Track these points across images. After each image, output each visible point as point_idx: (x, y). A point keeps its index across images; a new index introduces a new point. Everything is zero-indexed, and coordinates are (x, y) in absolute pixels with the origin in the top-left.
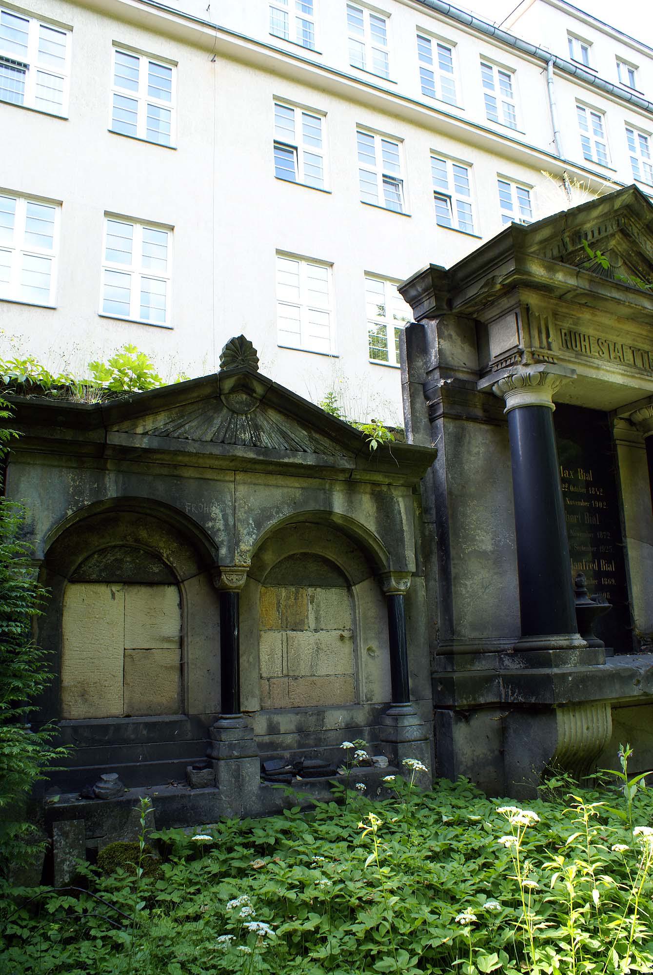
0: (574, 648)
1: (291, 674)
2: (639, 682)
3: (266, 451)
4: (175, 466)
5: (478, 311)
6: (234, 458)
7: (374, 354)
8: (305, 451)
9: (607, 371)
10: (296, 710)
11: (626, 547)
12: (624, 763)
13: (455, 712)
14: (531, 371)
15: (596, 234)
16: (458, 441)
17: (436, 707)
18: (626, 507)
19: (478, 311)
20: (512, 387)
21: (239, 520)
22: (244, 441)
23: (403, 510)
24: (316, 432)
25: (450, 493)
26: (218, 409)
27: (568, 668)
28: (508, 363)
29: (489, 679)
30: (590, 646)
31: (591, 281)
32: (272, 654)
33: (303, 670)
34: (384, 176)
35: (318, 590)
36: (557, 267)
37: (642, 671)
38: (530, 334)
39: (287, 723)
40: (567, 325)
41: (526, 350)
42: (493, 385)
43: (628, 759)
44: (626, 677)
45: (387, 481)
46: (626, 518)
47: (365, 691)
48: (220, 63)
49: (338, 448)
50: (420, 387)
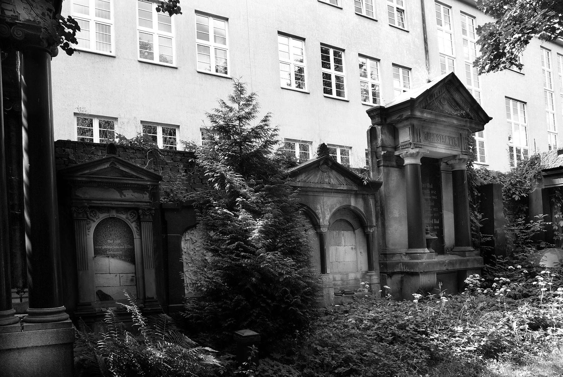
3: (333, 185)
4: (307, 192)
7: (326, 91)
9: (439, 148)
10: (340, 273)
12: (440, 287)
16: (387, 175)
17: (380, 273)
20: (407, 156)
22: (326, 182)
24: (347, 177)
25: (385, 196)
30: (431, 252)
39: (338, 277)
40: (426, 130)
50: (374, 153)
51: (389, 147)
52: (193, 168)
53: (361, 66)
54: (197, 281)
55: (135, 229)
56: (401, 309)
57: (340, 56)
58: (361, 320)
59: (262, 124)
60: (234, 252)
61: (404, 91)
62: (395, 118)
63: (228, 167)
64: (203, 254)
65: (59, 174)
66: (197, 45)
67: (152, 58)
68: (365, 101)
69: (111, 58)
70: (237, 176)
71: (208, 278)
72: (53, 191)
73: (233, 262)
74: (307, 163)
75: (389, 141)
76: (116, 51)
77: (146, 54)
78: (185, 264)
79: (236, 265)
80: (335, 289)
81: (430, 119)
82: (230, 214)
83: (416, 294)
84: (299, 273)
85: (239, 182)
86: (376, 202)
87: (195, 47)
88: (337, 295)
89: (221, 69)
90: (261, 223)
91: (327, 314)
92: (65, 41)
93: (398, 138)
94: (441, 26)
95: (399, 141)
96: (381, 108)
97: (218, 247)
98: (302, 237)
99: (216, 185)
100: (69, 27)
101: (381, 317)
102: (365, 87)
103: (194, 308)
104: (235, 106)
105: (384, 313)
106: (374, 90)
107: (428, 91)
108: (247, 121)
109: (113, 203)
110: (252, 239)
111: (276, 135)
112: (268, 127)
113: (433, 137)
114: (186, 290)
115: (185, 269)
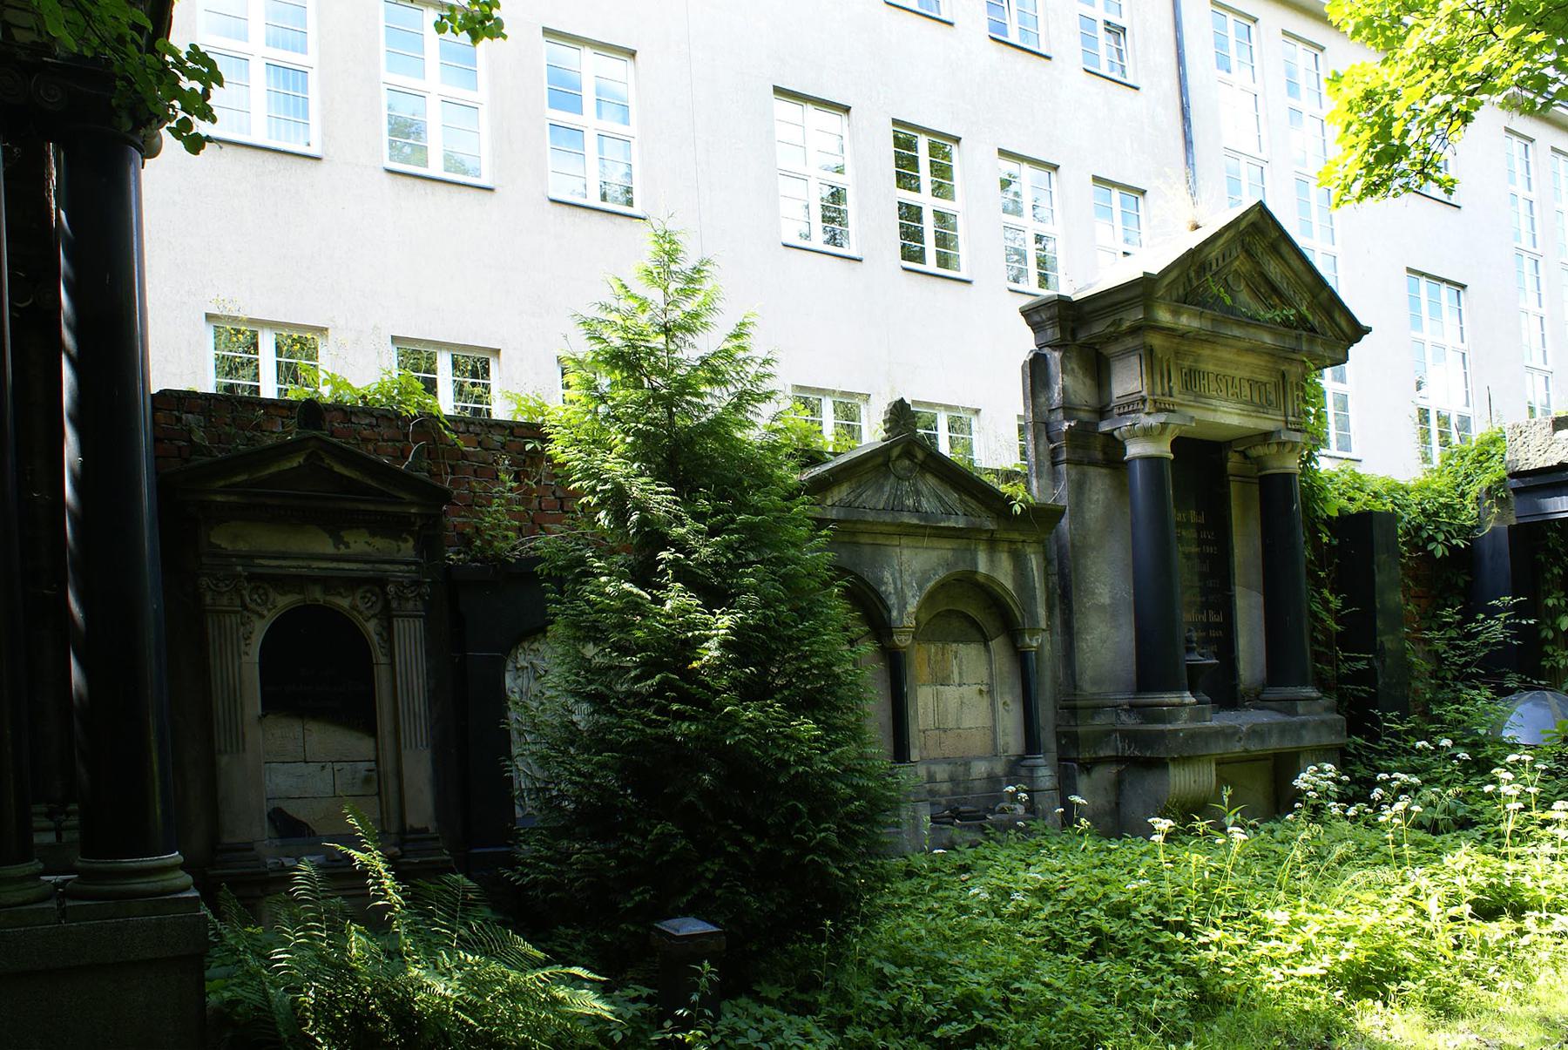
0: (1183, 705)
2: (1241, 739)
3: (925, 516)
4: (854, 533)
5: (1101, 343)
6: (900, 525)
7: (907, 254)
8: (957, 514)
10: (947, 760)
11: (1234, 596)
12: (1226, 800)
14: (1153, 421)
16: (1079, 488)
17: (1059, 760)
18: (1236, 551)
19: (1101, 343)
21: (907, 584)
22: (909, 507)
25: (1073, 545)
26: (886, 477)
27: (1179, 725)
29: (1108, 734)
30: (1199, 703)
36: (1182, 310)
37: (1244, 729)
39: (941, 772)
41: (1149, 398)
43: (1229, 797)
44: (1228, 734)
45: (1022, 538)
46: (1236, 564)
49: (983, 509)
52: (537, 467)
53: (1005, 184)
54: (548, 783)
55: (376, 638)
56: (1118, 860)
57: (947, 156)
59: (727, 345)
60: (653, 703)
62: (1099, 328)
63: (635, 466)
64: (564, 706)
65: (165, 487)
70: (660, 489)
71: (579, 773)
73: (648, 731)
75: (1082, 391)
77: (407, 150)
78: (514, 736)
79: (658, 738)
80: (932, 804)
82: (639, 596)
83: (1158, 819)
84: (834, 762)
85: (666, 507)
86: (1048, 561)
88: (938, 823)
91: (909, 874)
92: (181, 115)
96: (1063, 303)
97: (606, 687)
98: (841, 659)
99: (602, 514)
100: (192, 75)
103: (541, 858)
104: (656, 296)
106: (1041, 250)
107: (1191, 253)
108: (689, 337)
109: (315, 564)
110: (703, 667)
111: (770, 375)
112: (748, 354)
114: (517, 809)
115: (515, 751)
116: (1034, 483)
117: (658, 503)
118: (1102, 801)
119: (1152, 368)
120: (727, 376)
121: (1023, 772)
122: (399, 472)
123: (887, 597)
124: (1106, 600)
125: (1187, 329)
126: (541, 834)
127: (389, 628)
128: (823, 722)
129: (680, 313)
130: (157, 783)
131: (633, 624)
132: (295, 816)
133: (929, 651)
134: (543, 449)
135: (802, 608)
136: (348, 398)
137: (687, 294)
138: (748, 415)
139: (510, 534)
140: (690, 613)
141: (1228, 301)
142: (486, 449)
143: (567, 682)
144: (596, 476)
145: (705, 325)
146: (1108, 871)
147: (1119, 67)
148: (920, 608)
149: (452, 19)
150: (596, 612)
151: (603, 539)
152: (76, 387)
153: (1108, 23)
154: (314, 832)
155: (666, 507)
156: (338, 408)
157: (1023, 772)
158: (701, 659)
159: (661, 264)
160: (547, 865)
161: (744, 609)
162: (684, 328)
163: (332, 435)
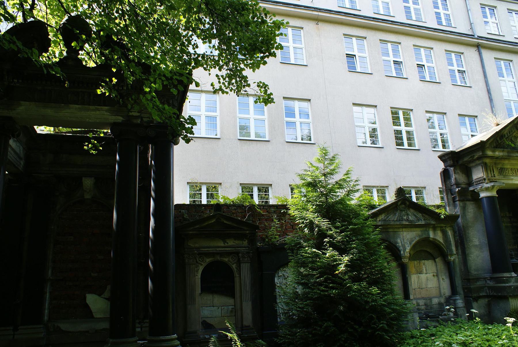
0: (513, 277)
1: (420, 287)
3: (411, 221)
8: (421, 220)
10: (423, 298)
13: (472, 298)
14: (489, 185)
15: (508, 134)
16: (464, 208)
17: (465, 297)
20: (482, 190)
21: (405, 243)
22: (405, 219)
23: (450, 234)
25: (463, 226)
26: (397, 210)
28: (480, 182)
31: (508, 152)
32: (414, 281)
33: (424, 286)
34: (394, 61)
35: (426, 261)
38: (487, 173)
39: (422, 302)
40: (499, 166)
42: (475, 189)
45: (445, 226)
47: (443, 292)
48: (320, 24)
50: (449, 191)
51: (463, 184)
52: (285, 217)
53: (428, 120)
54: (289, 311)
55: (235, 269)
56: (493, 332)
57: (409, 115)
58: (450, 344)
59: (344, 177)
60: (324, 285)
61: (472, 136)
62: (466, 159)
63: (316, 214)
64: (294, 287)
65: (176, 230)
66: (285, 122)
67: (250, 136)
68: (434, 148)
69: (217, 140)
70: (324, 221)
71: (299, 308)
72: (171, 242)
73: (322, 293)
74: (386, 205)
75: (462, 178)
76: (221, 134)
77: (244, 133)
78: (278, 297)
79: (325, 295)
80: (419, 313)
81: (503, 156)
82: (318, 252)
83: (508, 318)
84: (384, 301)
85: (326, 225)
86: (454, 232)
87: (284, 123)
88: (421, 319)
89: (305, 137)
90: (347, 258)
91: (412, 337)
92: (185, 134)
93: (472, 176)
94: (503, 77)
95: (472, 178)
96: (452, 153)
97: (308, 281)
98: (385, 268)
99: (306, 229)
100: (188, 124)
101: (471, 341)
102: (434, 137)
103: (287, 334)
104: (321, 165)
105: (473, 336)
106: (442, 137)
107: (497, 133)
108: (332, 176)
109: (218, 249)
110: (339, 273)
111: (358, 185)
112: (350, 179)
113: (507, 171)
114: (278, 319)
115: (278, 301)
116: (448, 208)
117: (324, 225)
118: (482, 311)
119: (487, 169)
120: (344, 186)
121: (452, 301)
122: (244, 222)
123: (399, 247)
124: (477, 243)
125: (498, 156)
126: (287, 327)
127: (240, 266)
128: (380, 288)
129: (329, 170)
130: (171, 313)
131: (317, 261)
132: (209, 323)
133: (414, 263)
134: (287, 212)
135: (371, 253)
136: (228, 202)
137: (331, 164)
138: (351, 197)
139: (277, 237)
140: (335, 257)
141: (513, 145)
142: (269, 213)
143: (295, 280)
144: (304, 219)
145: (336, 172)
146: (490, 336)
147: (464, 82)
148: (411, 250)
149: (259, 99)
150: (304, 258)
151: (306, 236)
152: (154, 205)
153: (459, 70)
154: (215, 327)
155: (326, 225)
156: (226, 205)
157: (452, 301)
158: (339, 270)
159: (323, 157)
160: (289, 337)
161: (353, 254)
162: (330, 174)
163: (224, 212)
